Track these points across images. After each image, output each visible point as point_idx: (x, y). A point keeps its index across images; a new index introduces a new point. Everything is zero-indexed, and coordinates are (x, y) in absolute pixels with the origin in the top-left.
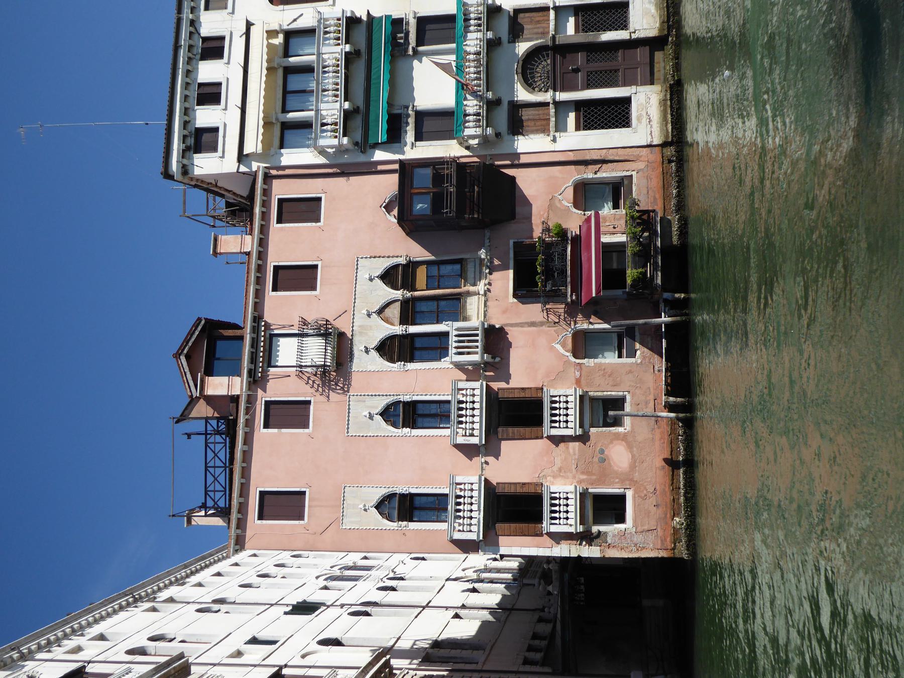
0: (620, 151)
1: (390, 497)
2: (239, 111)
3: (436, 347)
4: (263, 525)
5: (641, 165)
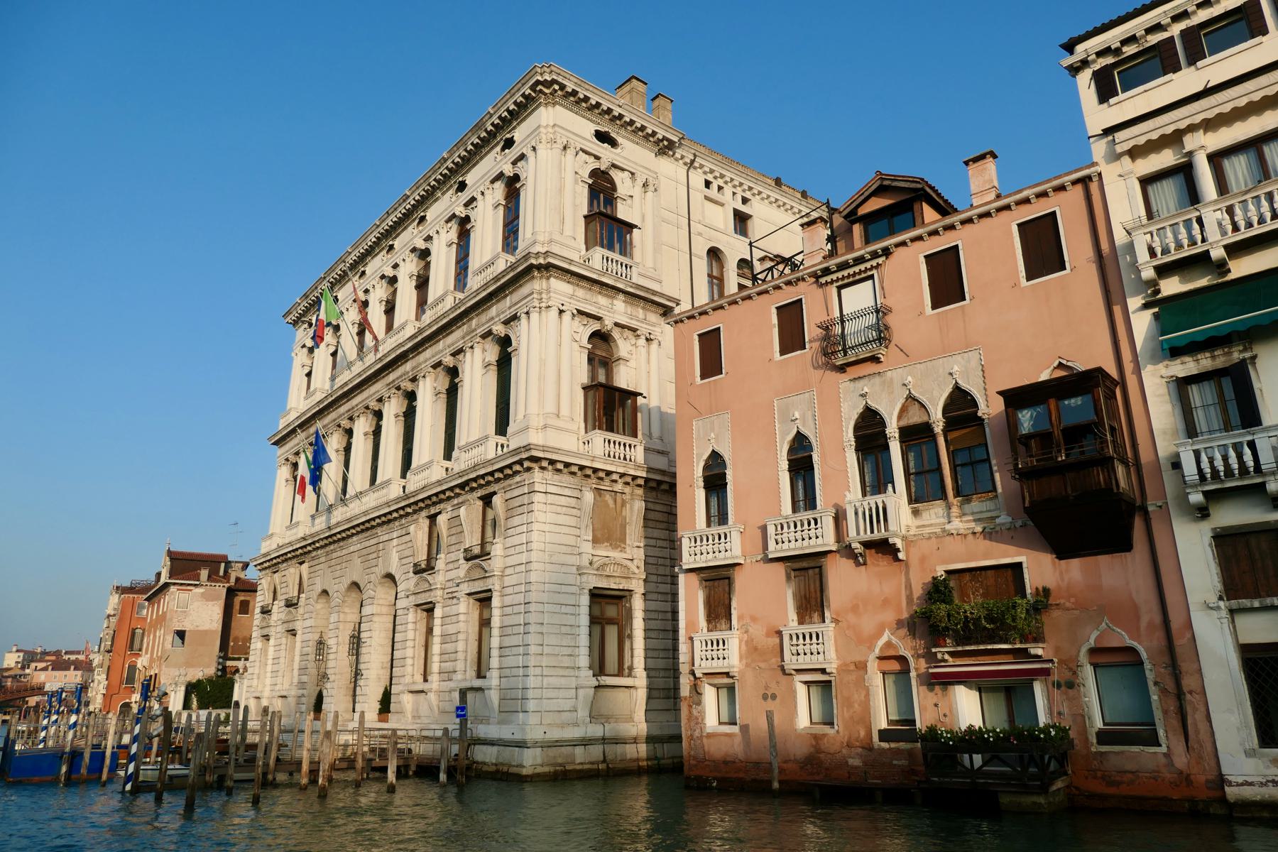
0: (1199, 716)
1: (723, 464)
2: (1201, 88)
3: (877, 480)
4: (692, 340)
5: (1181, 760)
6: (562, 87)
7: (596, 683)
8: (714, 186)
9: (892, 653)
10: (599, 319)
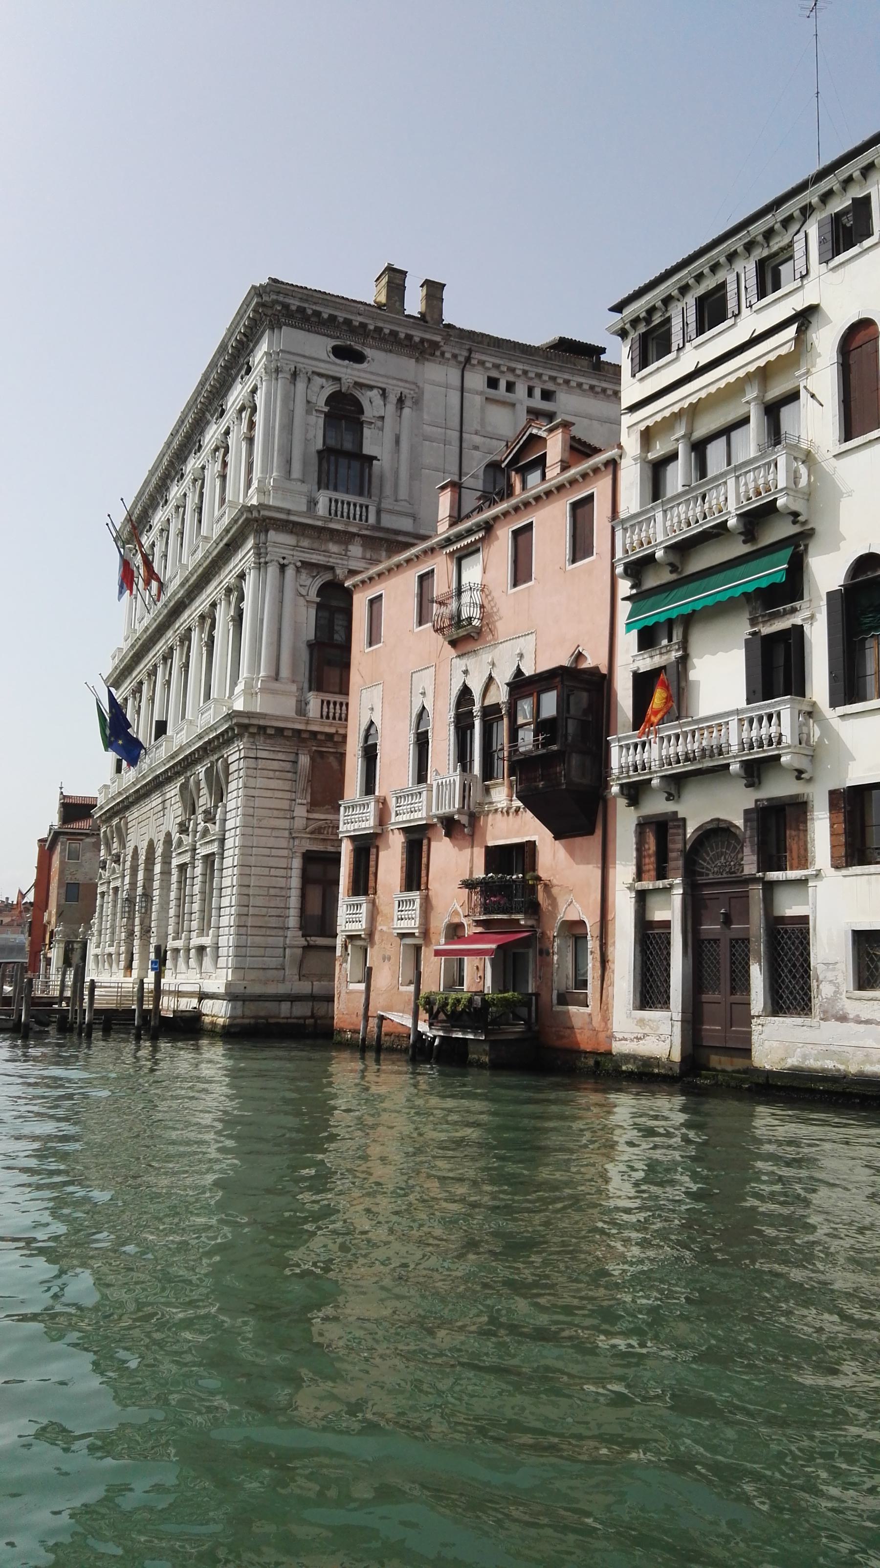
6: (286, 306)
7: (305, 943)
8: (503, 384)
10: (332, 569)
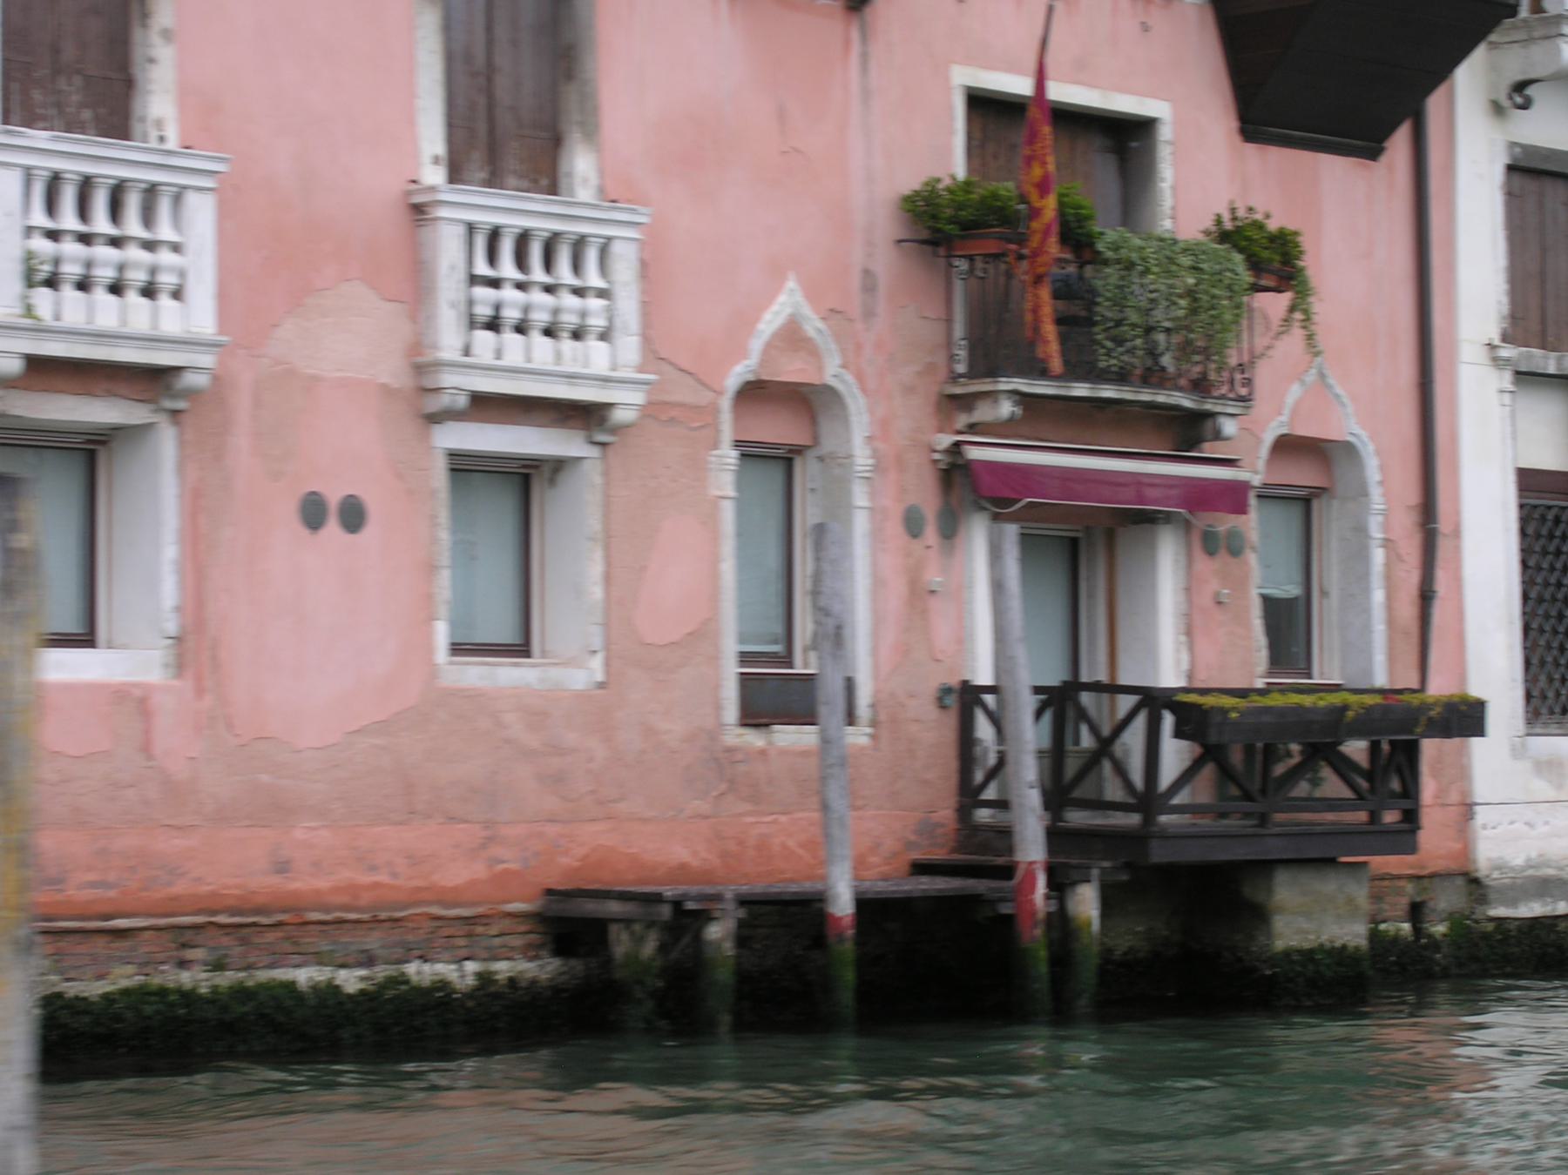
9: (791, 371)
